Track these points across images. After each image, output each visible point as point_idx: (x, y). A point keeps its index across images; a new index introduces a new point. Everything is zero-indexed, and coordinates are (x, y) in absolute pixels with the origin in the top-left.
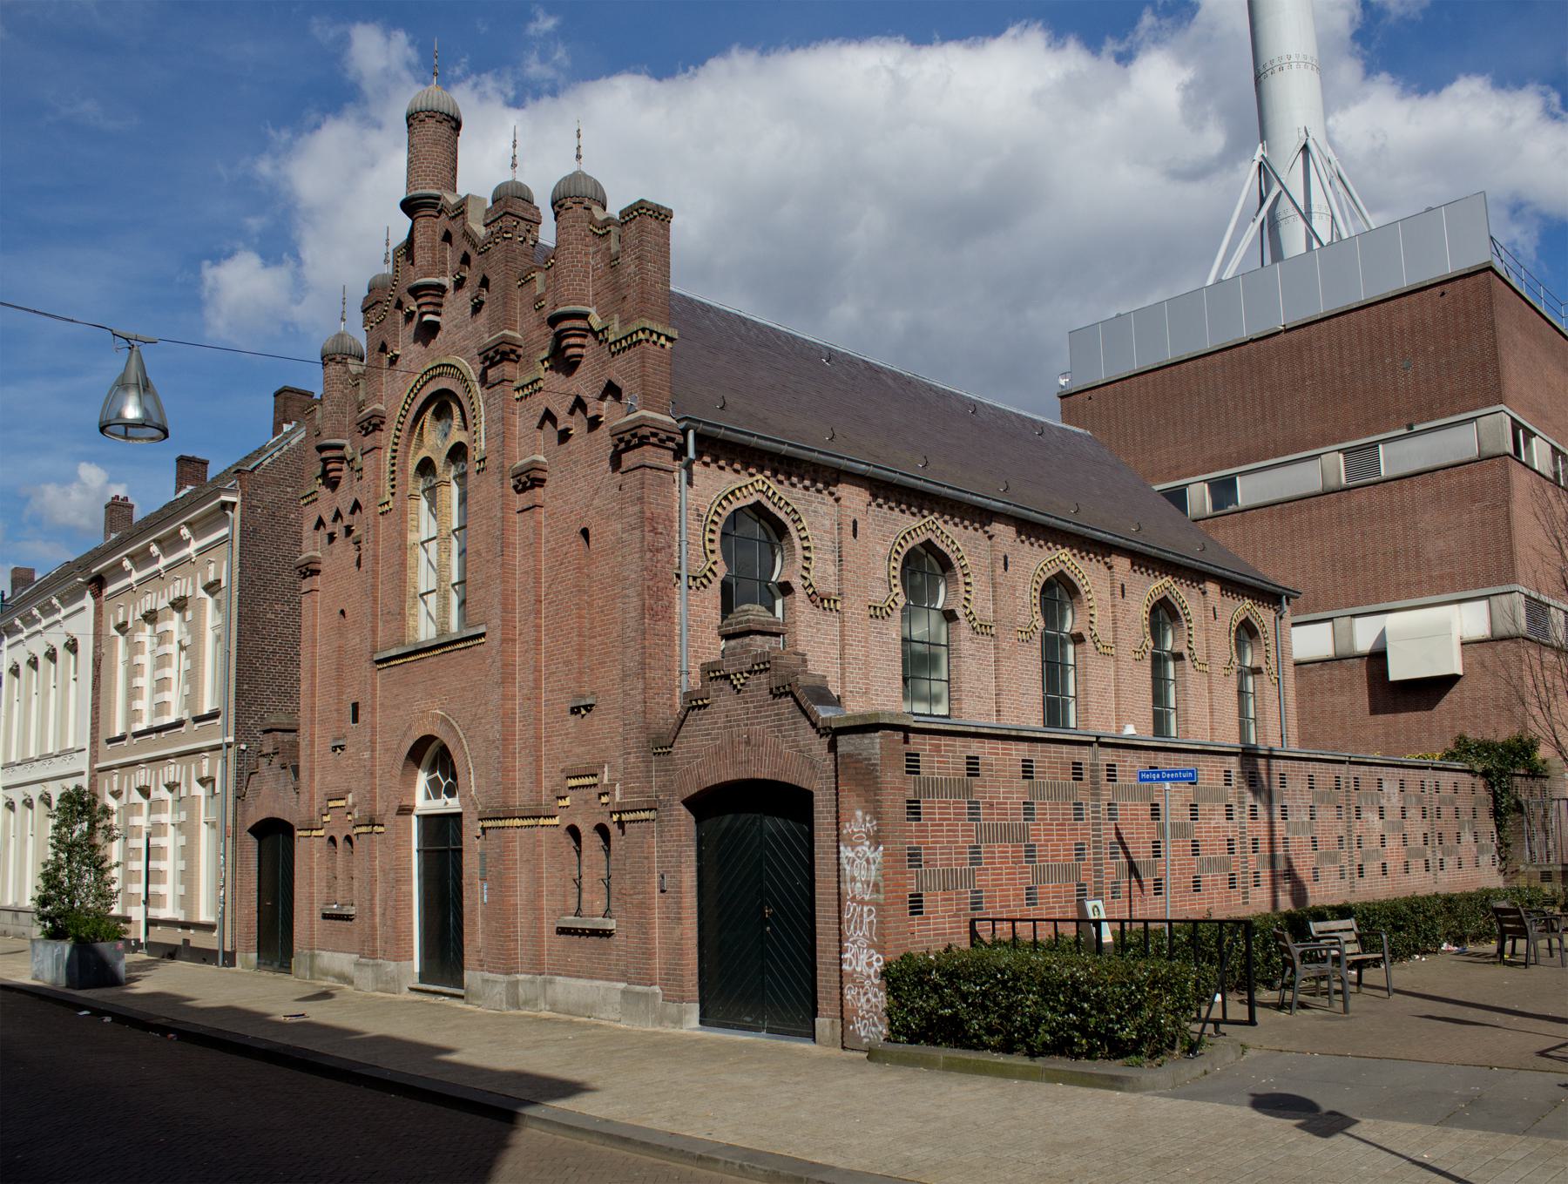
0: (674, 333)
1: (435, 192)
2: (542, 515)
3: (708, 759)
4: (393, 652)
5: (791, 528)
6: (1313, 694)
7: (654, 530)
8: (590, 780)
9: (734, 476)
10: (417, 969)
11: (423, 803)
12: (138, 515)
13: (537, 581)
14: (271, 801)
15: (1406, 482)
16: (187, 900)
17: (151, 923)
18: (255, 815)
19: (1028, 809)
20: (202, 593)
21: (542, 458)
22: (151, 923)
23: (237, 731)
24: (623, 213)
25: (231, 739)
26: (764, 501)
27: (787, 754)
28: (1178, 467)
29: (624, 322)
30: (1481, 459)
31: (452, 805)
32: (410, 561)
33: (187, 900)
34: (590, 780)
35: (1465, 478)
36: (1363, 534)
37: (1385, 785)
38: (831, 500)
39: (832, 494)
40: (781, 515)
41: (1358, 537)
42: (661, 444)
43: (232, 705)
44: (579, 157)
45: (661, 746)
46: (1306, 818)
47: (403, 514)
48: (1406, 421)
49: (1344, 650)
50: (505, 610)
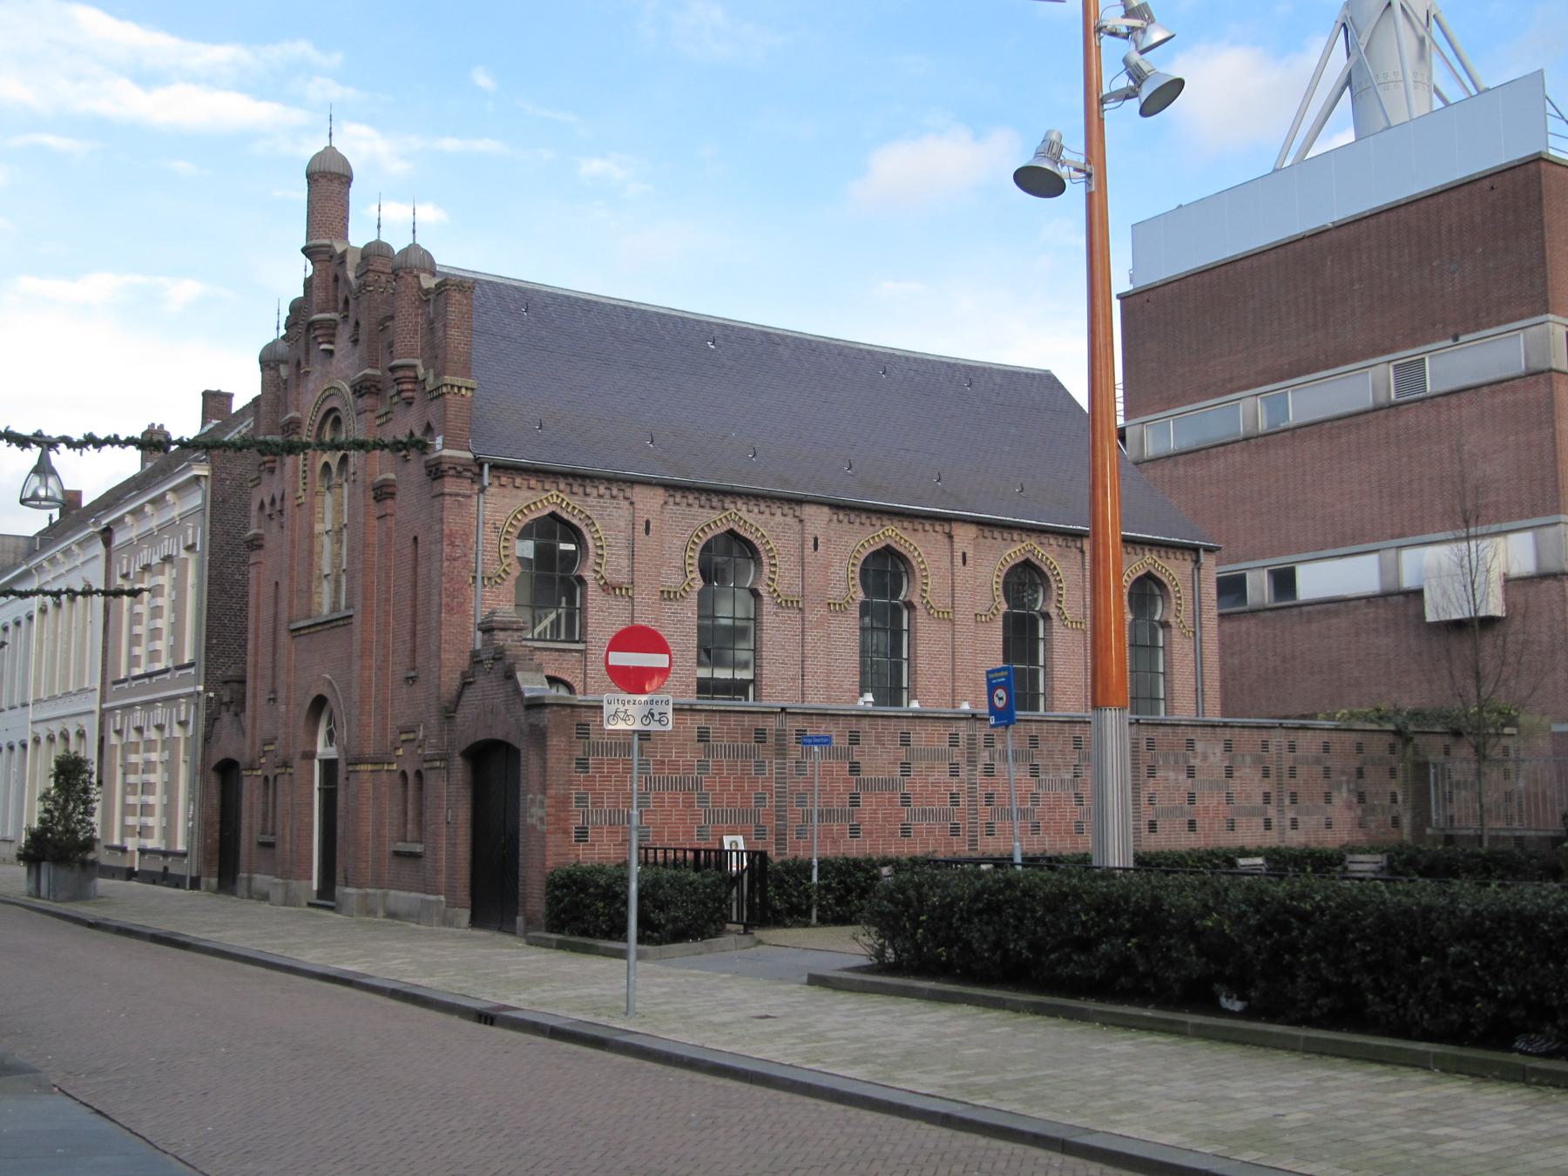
0: (471, 383)
1: (327, 242)
2: (391, 522)
4: (302, 624)
5: (585, 530)
6: (1358, 634)
7: (452, 544)
9: (529, 494)
10: (315, 887)
11: (323, 750)
13: (388, 577)
14: (227, 748)
15: (1454, 400)
16: (169, 832)
18: (217, 757)
19: (703, 766)
20: (183, 554)
21: (392, 476)
25: (201, 688)
26: (559, 511)
28: (1231, 380)
29: (437, 376)
30: (1375, 410)
32: (317, 549)
33: (169, 832)
34: (411, 736)
35: (1509, 398)
36: (1410, 456)
38: (625, 504)
39: (626, 498)
40: (575, 521)
41: (1405, 460)
42: (459, 475)
43: (203, 657)
45: (449, 712)
46: (1069, 776)
47: (312, 508)
48: (1451, 331)
49: (1392, 587)
50: (365, 599)
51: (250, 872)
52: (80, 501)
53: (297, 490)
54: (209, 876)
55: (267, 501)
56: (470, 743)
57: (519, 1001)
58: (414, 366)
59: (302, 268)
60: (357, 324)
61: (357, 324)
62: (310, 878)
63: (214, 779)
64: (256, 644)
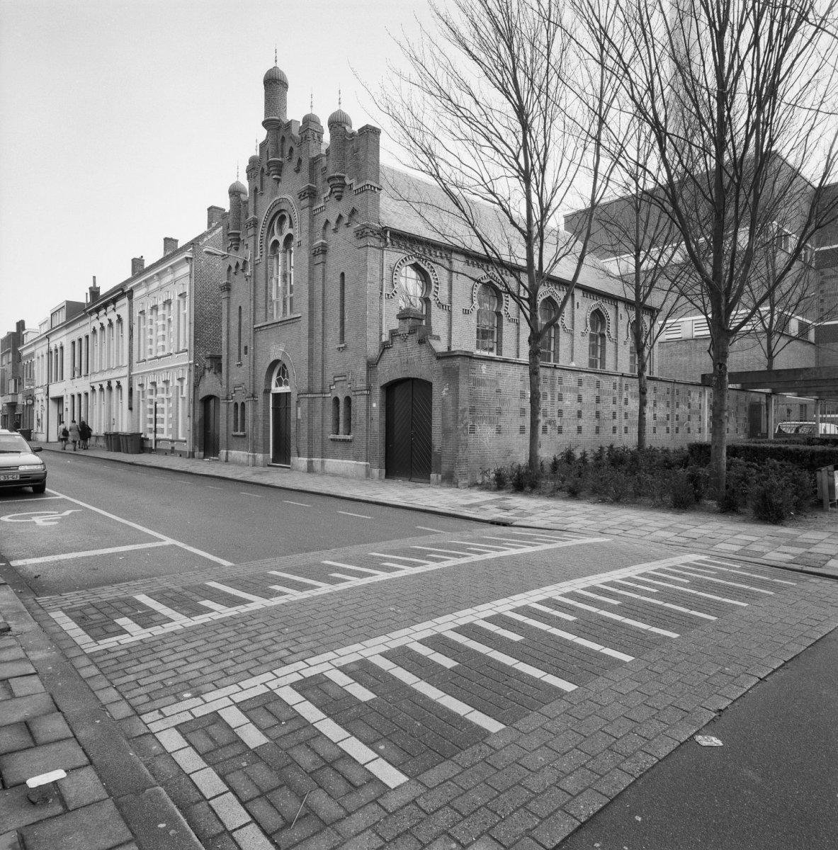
3: (390, 370)
8: (343, 378)
12: (146, 265)
14: (210, 385)
17: (157, 441)
18: (203, 393)
22: (157, 441)
23: (195, 358)
24: (360, 130)
27: (422, 368)
31: (283, 389)
34: (343, 378)
37: (692, 394)
44: (340, 103)
51: (228, 449)
52: (99, 292)
53: (255, 256)
54: (200, 451)
55: (233, 266)
56: (388, 380)
57: (122, 459)
58: (343, 178)
59: (262, 134)
60: (300, 161)
61: (300, 161)
62: (269, 453)
63: (198, 405)
64: (228, 339)
